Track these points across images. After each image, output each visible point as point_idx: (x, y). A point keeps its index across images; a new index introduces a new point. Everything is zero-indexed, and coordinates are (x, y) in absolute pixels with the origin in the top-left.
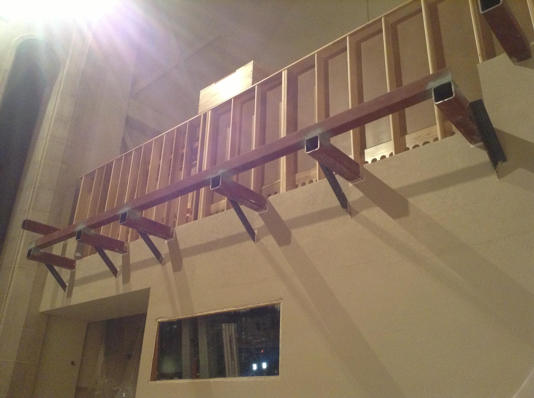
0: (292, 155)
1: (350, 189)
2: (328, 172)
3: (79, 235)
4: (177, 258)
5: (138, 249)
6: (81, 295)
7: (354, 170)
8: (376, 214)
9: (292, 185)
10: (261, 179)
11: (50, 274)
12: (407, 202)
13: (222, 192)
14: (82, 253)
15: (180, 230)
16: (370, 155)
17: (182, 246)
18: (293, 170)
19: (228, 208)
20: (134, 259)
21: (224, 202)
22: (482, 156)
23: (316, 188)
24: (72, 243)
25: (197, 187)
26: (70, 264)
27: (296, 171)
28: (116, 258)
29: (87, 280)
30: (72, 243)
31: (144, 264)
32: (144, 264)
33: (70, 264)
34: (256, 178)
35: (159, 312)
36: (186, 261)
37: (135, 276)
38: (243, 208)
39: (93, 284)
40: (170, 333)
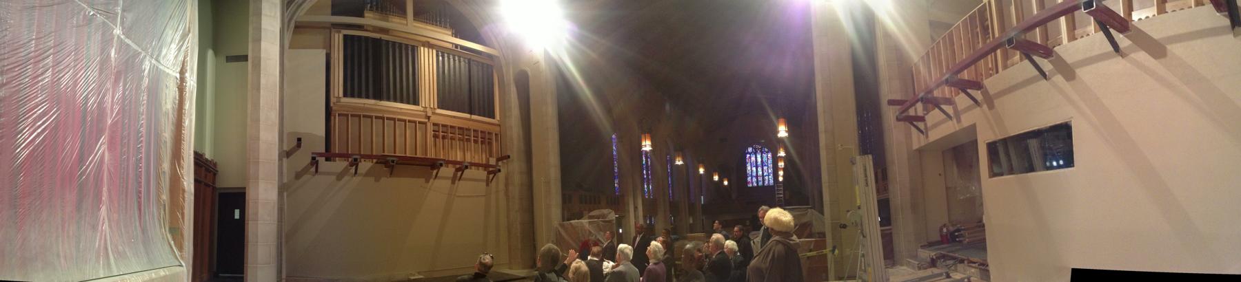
0: (1069, 15)
1: (1120, 38)
2: (1103, 26)
3: (922, 100)
4: (990, 101)
5: (962, 100)
6: (934, 135)
7: (1124, 25)
8: (1142, 56)
9: (1072, 37)
10: (1046, 36)
11: (913, 129)
12: (1165, 49)
13: (1015, 48)
14: (927, 111)
15: (987, 82)
16: (1135, 16)
17: (992, 92)
18: (1072, 27)
19: (1021, 60)
20: (960, 107)
21: (1017, 57)
23: (1092, 38)
24: (919, 106)
25: (994, 50)
26: (922, 119)
27: (1075, 29)
28: (949, 109)
29: (935, 126)
30: (919, 106)
31: (968, 109)
32: (968, 109)
33: (922, 119)
34: (1041, 35)
35: (985, 137)
36: (996, 102)
37: (963, 117)
38: (1035, 58)
39: (940, 127)
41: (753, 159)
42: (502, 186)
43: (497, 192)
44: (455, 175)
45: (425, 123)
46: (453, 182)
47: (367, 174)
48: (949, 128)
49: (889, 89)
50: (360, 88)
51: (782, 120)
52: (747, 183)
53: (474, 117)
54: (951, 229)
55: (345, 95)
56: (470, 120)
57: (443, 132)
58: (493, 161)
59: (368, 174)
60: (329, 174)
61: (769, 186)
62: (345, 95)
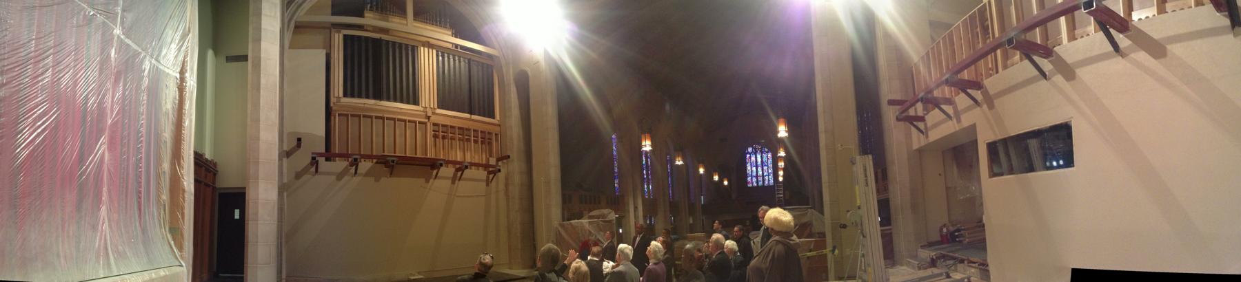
0: (1069, 15)
1: (1120, 38)
2: (1103, 26)
3: (922, 100)
4: (990, 101)
5: (962, 100)
6: (934, 135)
7: (1124, 25)
8: (1142, 56)
9: (1072, 37)
10: (1046, 36)
11: (913, 129)
12: (1165, 49)
13: (1015, 48)
14: (927, 111)
15: (987, 82)
16: (1135, 16)
17: (992, 92)
18: (1072, 27)
19: (1021, 60)
20: (960, 107)
21: (1017, 57)
22: (1227, 22)
23: (1092, 38)
24: (919, 106)
25: (994, 50)
26: (922, 119)
27: (1075, 29)
28: (949, 109)
29: (935, 126)
30: (919, 106)
31: (968, 109)
32: (968, 109)
33: (922, 119)
34: (1041, 35)
35: (985, 137)
36: (996, 102)
37: (963, 117)
38: (1035, 58)
39: (940, 127)
40: (992, 147)
41: (753, 159)
42: (502, 186)
43: (497, 192)
44: (455, 175)
45: (425, 123)
46: (453, 182)
47: (367, 174)
48: (949, 128)
49: (889, 89)
50: (360, 88)
51: (782, 120)
52: (747, 183)
53: (474, 117)
54: (951, 229)
55: (345, 95)
56: (470, 120)
57: (443, 132)
58: (493, 161)
59: (368, 174)
60: (329, 174)
61: (769, 186)
62: (345, 95)
